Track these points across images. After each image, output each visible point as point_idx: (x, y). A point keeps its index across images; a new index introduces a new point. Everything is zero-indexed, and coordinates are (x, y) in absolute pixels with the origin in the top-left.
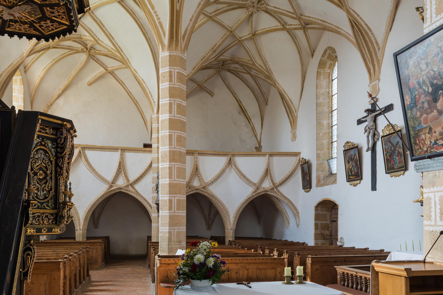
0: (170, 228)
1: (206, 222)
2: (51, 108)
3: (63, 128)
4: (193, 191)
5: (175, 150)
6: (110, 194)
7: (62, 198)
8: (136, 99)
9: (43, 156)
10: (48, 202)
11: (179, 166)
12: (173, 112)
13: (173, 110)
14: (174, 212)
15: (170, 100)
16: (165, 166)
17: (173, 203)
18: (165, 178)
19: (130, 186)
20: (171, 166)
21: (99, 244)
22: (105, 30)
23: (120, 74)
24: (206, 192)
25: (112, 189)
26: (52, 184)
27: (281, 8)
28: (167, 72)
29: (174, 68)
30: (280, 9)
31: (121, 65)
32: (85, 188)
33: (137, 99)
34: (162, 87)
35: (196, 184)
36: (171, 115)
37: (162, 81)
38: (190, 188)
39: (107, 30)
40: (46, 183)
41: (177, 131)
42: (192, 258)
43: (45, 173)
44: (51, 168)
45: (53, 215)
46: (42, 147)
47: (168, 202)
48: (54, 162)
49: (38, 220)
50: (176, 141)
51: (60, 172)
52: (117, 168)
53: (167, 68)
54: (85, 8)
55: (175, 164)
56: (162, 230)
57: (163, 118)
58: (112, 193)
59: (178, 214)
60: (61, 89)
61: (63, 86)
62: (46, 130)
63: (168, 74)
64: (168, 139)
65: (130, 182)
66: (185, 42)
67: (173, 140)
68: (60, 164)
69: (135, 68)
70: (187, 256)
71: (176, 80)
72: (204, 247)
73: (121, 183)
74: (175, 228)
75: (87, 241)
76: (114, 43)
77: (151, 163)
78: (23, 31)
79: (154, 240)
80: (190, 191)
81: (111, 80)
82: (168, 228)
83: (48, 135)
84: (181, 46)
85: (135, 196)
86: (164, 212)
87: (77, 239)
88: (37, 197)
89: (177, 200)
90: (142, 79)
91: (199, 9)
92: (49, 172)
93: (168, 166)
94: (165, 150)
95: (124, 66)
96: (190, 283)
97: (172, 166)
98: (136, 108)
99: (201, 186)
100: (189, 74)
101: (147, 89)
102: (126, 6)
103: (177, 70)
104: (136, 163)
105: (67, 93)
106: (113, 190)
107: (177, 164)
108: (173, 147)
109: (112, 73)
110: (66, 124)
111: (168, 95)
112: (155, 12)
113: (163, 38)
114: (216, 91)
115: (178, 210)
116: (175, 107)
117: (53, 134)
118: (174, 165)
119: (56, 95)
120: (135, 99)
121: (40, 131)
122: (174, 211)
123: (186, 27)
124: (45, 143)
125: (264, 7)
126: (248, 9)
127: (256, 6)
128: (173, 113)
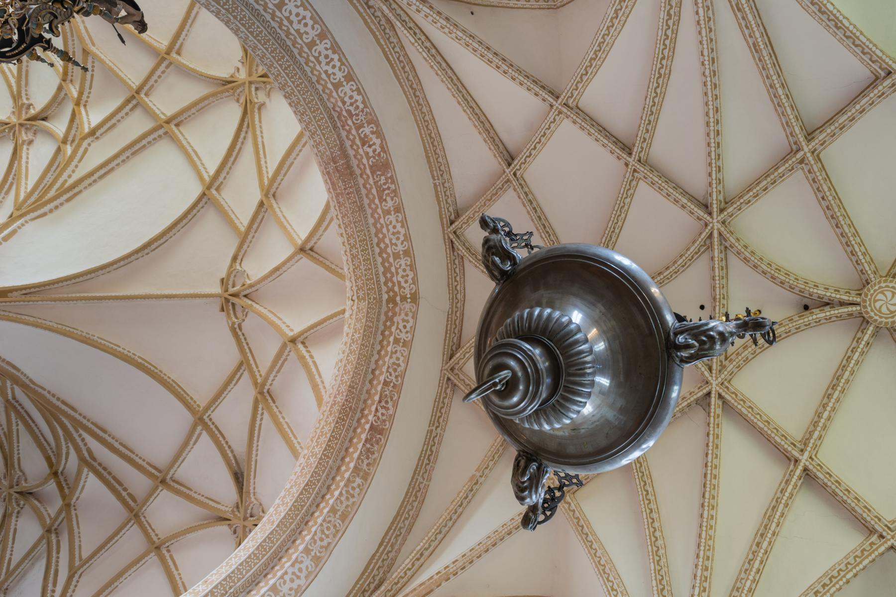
27: (15, 546)
30: (13, 543)
125: (13, 509)
126: (5, 478)
127: (12, 491)
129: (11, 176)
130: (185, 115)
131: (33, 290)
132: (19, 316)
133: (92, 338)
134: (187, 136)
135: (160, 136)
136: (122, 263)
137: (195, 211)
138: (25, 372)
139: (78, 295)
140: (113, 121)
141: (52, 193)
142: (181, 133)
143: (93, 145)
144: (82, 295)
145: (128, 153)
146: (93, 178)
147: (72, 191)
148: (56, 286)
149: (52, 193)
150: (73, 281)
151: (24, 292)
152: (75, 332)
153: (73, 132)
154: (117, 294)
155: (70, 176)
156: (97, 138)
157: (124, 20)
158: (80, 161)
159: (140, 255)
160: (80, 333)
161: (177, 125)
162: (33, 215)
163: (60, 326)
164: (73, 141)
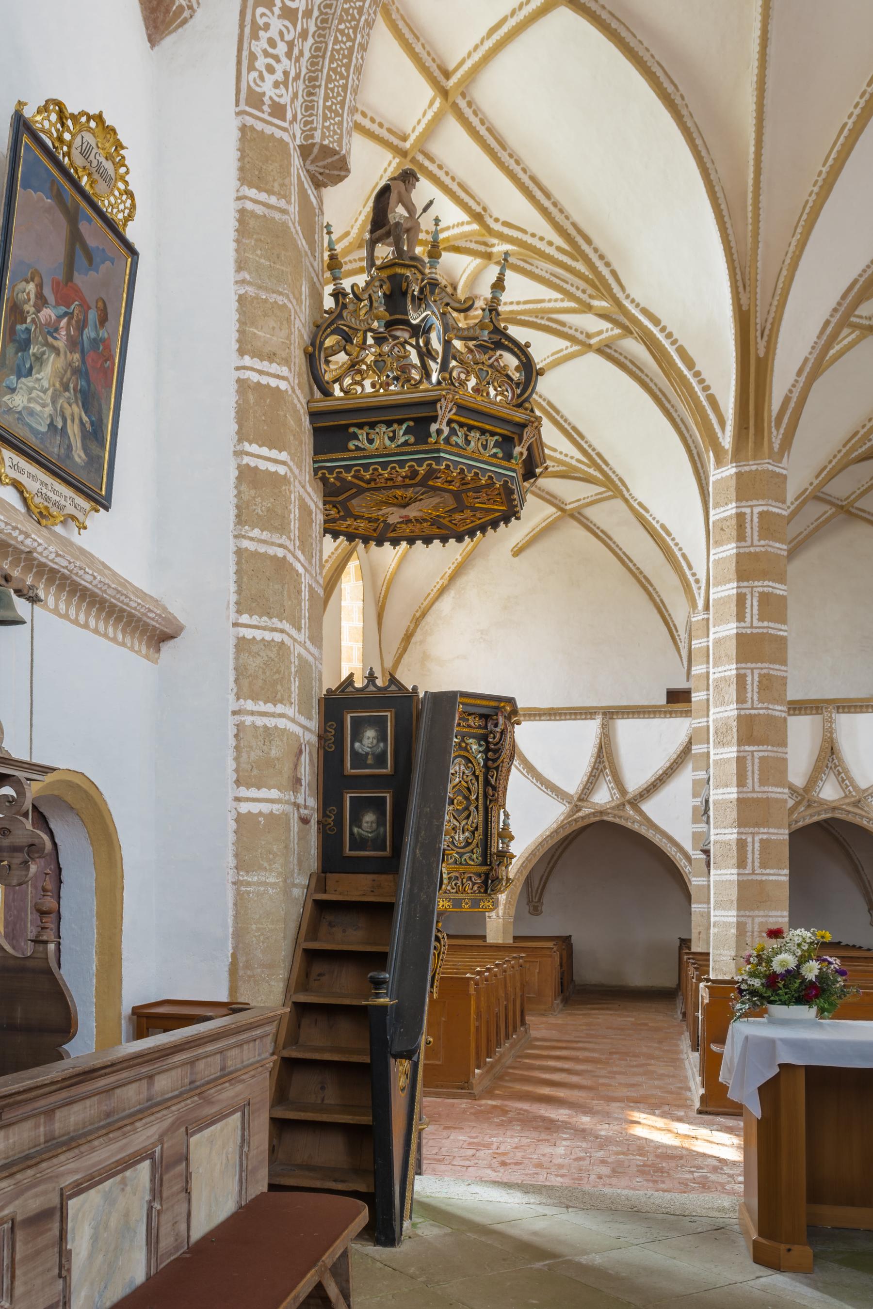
0: (742, 913)
2: (423, 623)
3: (499, 714)
5: (753, 712)
6: (575, 827)
7: (498, 845)
9: (462, 768)
10: (472, 852)
11: (766, 754)
12: (748, 615)
13: (748, 610)
14: (753, 873)
15: (738, 587)
16: (725, 756)
17: (750, 849)
18: (727, 786)
19: (628, 807)
20: (742, 754)
21: (548, 952)
22: (562, 421)
23: (596, 515)
24: (862, 817)
25: (580, 814)
26: (477, 818)
28: (731, 517)
29: (750, 503)
31: (601, 493)
32: (529, 819)
34: (716, 557)
36: (742, 624)
37: (716, 542)
38: (809, 806)
39: (566, 421)
40: (468, 817)
41: (759, 665)
42: (769, 961)
43: (467, 798)
44: (477, 788)
45: (480, 877)
46: (462, 753)
47: (734, 847)
48: (481, 778)
49: (456, 885)
50: (756, 689)
51: (493, 795)
53: (730, 506)
54: (537, 467)
55: (755, 748)
56: (717, 919)
57: (720, 635)
58: (580, 824)
59: (764, 878)
60: (447, 575)
61: (453, 567)
62: (468, 720)
63: (734, 522)
64: (734, 687)
65: (627, 798)
66: (782, 431)
67: (749, 687)
68: (493, 781)
69: (641, 498)
70: (758, 956)
71: (756, 534)
72: (796, 939)
73: (603, 796)
74: (756, 913)
75: (516, 945)
76: (585, 446)
77: (690, 743)
78: (417, 532)
79: (697, 947)
80: (811, 816)
81: (575, 532)
82: (734, 913)
83: (471, 730)
84: (770, 443)
85: (643, 831)
86: (723, 872)
87: (490, 940)
88: (453, 843)
89: (762, 841)
90: (663, 527)
91: (825, 337)
92: (473, 797)
93: (735, 755)
94: (726, 714)
95: (610, 493)
96: (766, 1011)
97: (745, 754)
98: (646, 597)
99: (847, 801)
101: (676, 549)
102: (616, 355)
103: (760, 509)
104: (645, 747)
105: (461, 581)
106: (583, 818)
107: (761, 748)
108: (749, 705)
109: (577, 516)
110: (504, 707)
111: (733, 576)
112: (697, 374)
113: (720, 434)
115: (765, 868)
116: (753, 605)
117: (480, 727)
118: (752, 752)
119: (435, 590)
120: (641, 573)
121: (459, 725)
122: (753, 869)
123: (785, 391)
124: (467, 744)
128: (748, 619)
129: (539, 321)
130: (429, 63)
131: (739, 277)
132: (779, 291)
133: (824, 176)
134: (464, 53)
135: (470, 104)
136: (698, 142)
137: (605, 15)
138: (859, 271)
139: (750, 208)
140: (455, 187)
141: (580, 266)
142: (463, 62)
143: (495, 215)
144: (750, 201)
145: (504, 156)
146: (551, 208)
147: (575, 238)
148: (733, 244)
149: (580, 266)
150: (726, 219)
151: (741, 289)
152: (810, 204)
153: (473, 246)
154: (752, 142)
155: (550, 243)
156: (485, 209)
157: (410, 208)
158: (524, 231)
159: (684, 112)
160: (814, 197)
161: (447, 75)
162: (616, 289)
163: (799, 230)
164: (485, 244)
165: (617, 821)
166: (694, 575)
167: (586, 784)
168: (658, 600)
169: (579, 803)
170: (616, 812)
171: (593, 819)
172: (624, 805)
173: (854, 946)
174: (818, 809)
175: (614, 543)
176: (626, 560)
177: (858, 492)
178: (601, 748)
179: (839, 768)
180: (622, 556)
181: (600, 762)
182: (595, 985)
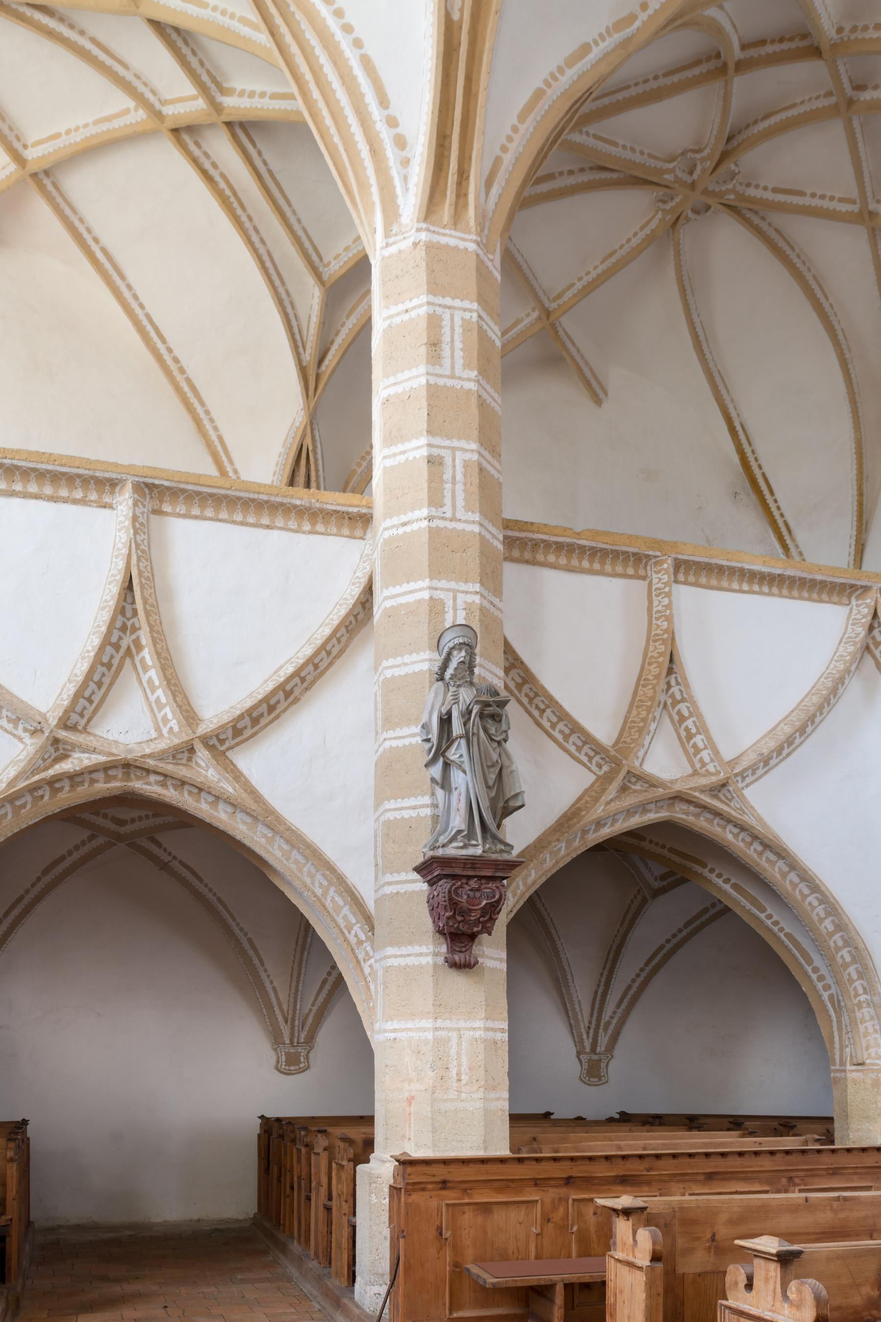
1: (578, 1042)
4: (643, 808)
8: (191, 373)
19: (203, 755)
25: (66, 766)
33: (196, 371)
35: (662, 761)
38: (624, 789)
52: (106, 616)
65: (201, 730)
73: (132, 726)
85: (239, 827)
100: (633, 17)
104: (247, 599)
106: (74, 778)
114: (615, 377)
120: (182, 371)
165: (170, 795)
166: (392, 122)
167: (85, 685)
168: (213, 437)
169: (63, 734)
170: (169, 768)
171: (103, 787)
172: (192, 750)
173: (580, 1120)
174: (642, 798)
175: (129, 287)
176: (153, 334)
177: (579, 285)
178: (129, 587)
179: (682, 707)
180: (145, 322)
181: (124, 628)
182: (79, 1228)
